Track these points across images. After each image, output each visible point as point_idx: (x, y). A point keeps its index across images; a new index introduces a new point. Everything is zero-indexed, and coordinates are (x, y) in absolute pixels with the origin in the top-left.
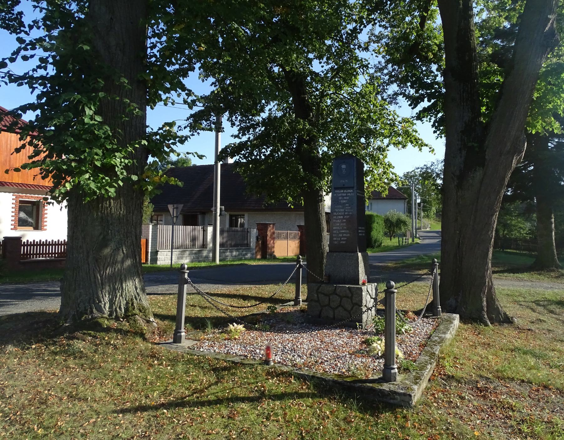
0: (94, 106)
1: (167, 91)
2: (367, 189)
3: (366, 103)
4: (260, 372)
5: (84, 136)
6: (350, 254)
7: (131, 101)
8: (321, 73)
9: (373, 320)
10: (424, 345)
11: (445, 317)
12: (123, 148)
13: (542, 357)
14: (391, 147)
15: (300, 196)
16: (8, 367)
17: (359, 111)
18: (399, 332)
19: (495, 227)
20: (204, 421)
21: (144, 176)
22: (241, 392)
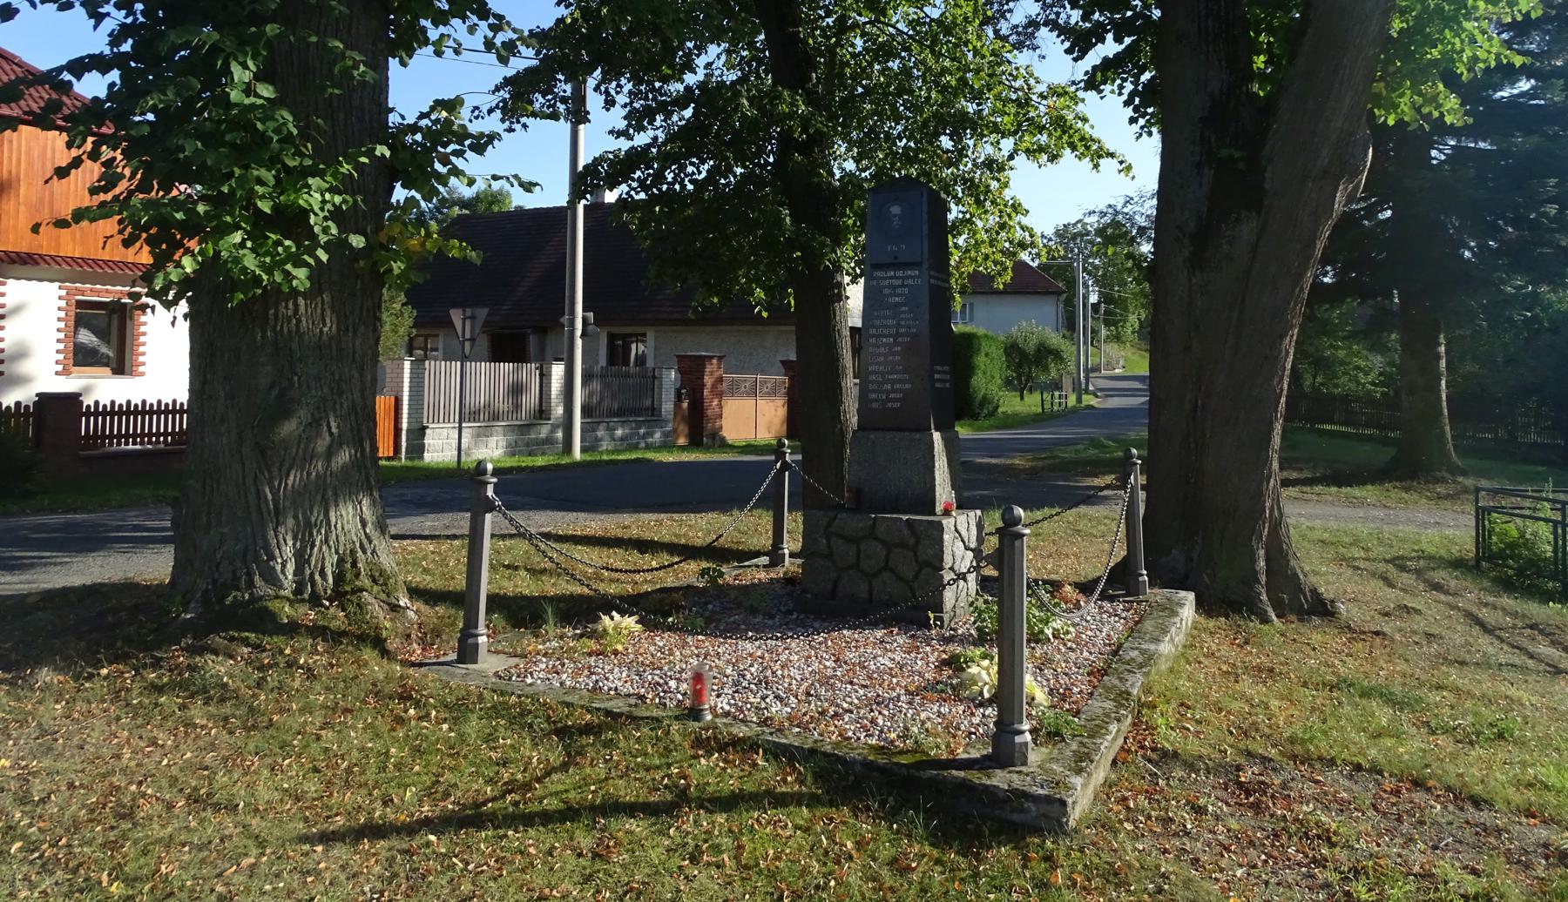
0: (253, 58)
1: (441, 19)
2: (957, 268)
3: (956, 46)
4: (677, 738)
5: (228, 137)
7: (346, 47)
9: (971, 604)
10: (1103, 672)
11: (1158, 598)
12: (328, 166)
13: (1409, 704)
14: (1021, 159)
16: (40, 725)
17: (936, 68)
18: (1036, 638)
19: (1289, 366)
20: (532, 864)
21: (383, 237)
22: (627, 791)
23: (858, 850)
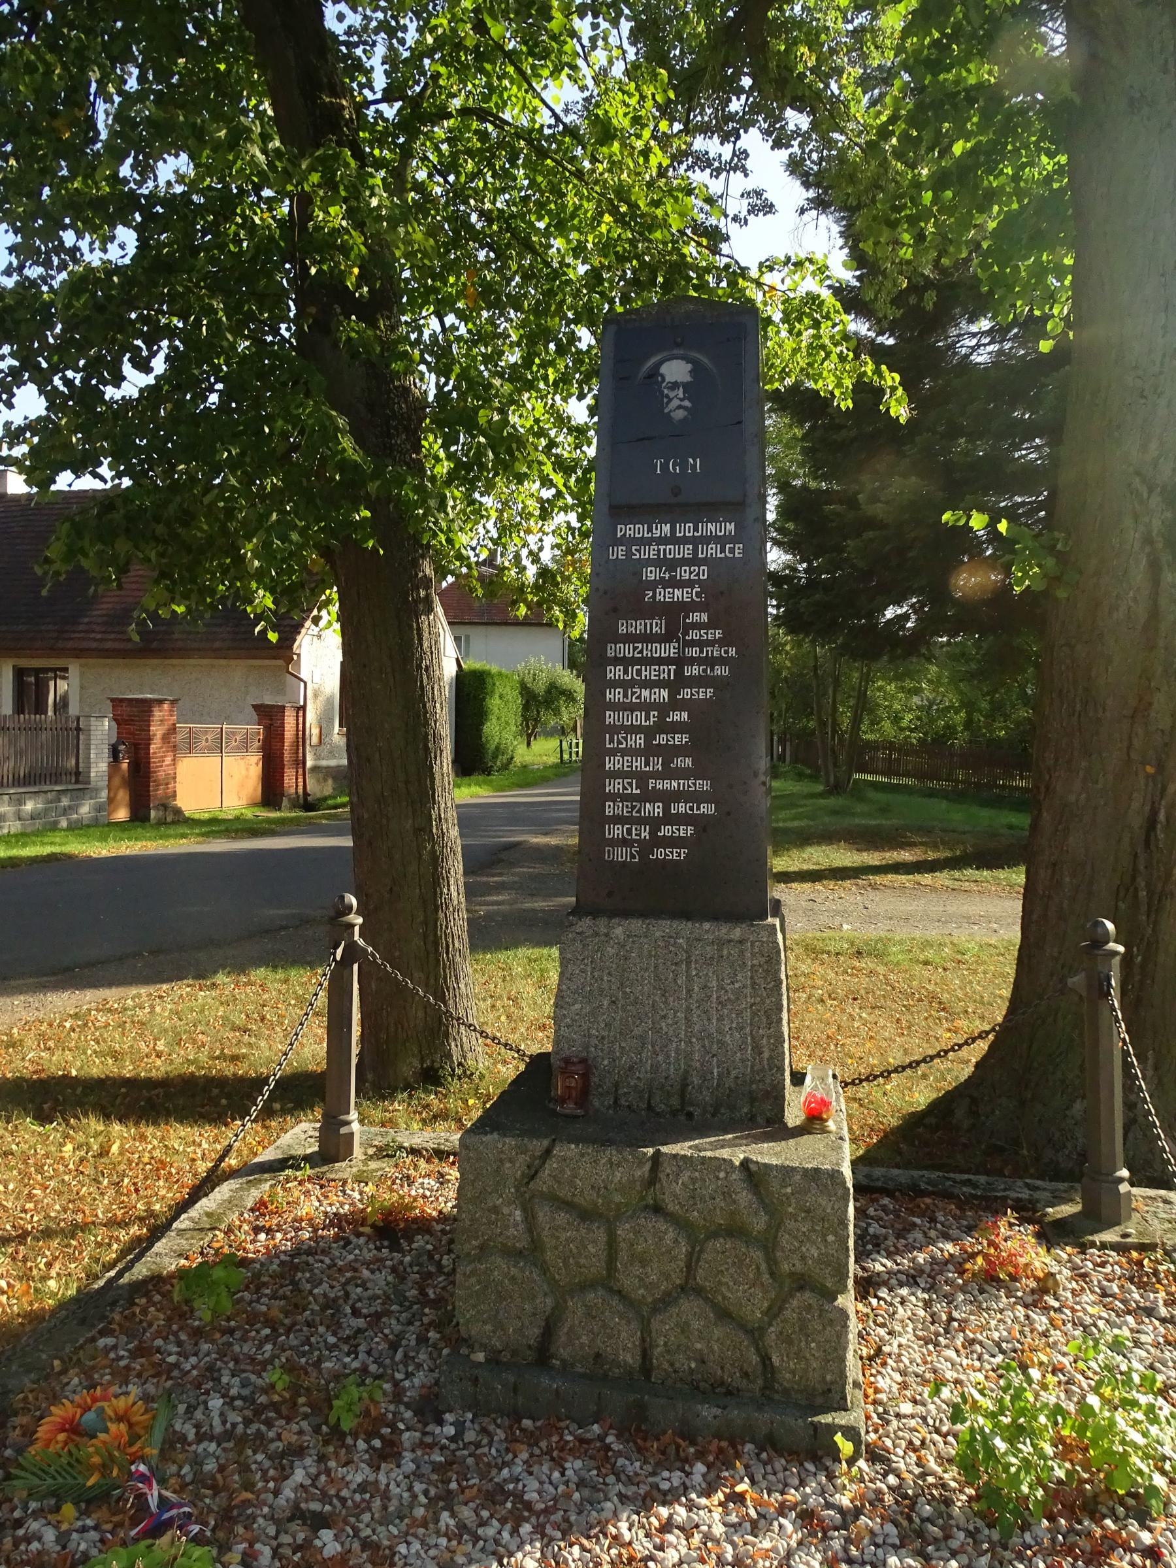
6: (724, 930)
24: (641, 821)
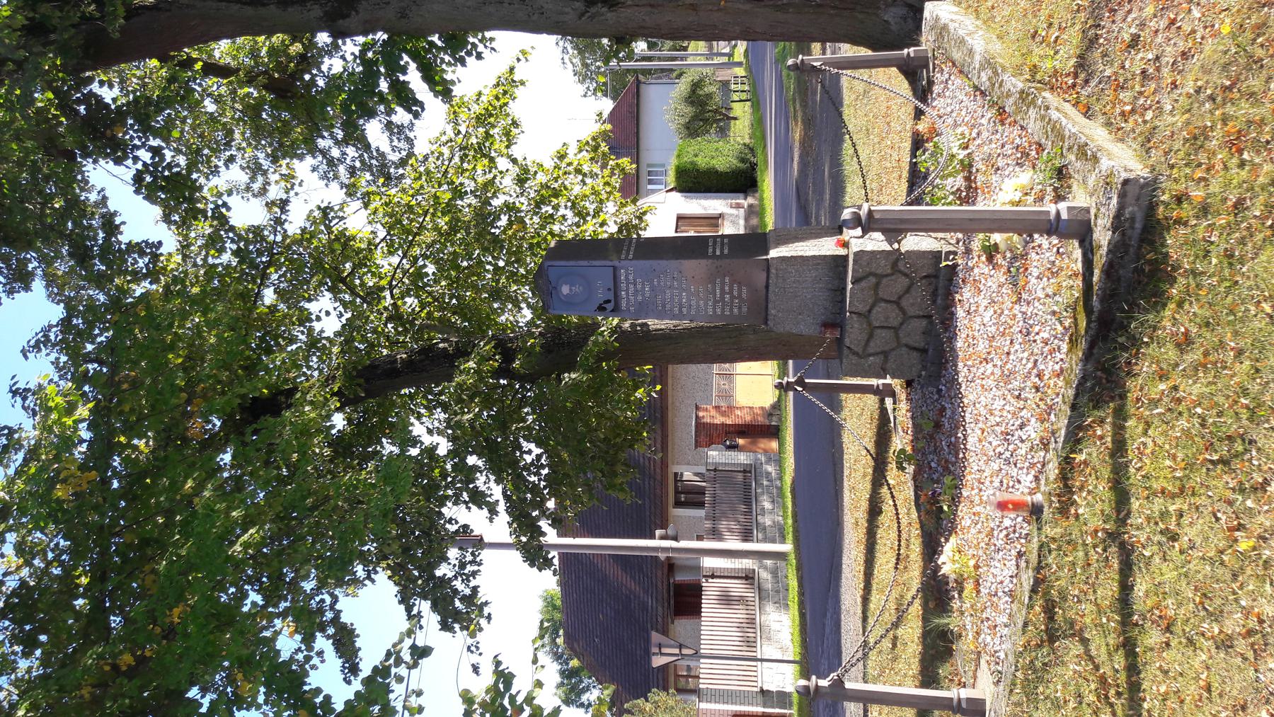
8: (344, 320)
10: (1001, 111)
14: (516, 151)
15: (633, 374)
22: (1108, 589)
23: (1167, 379)
24: (732, 302)
